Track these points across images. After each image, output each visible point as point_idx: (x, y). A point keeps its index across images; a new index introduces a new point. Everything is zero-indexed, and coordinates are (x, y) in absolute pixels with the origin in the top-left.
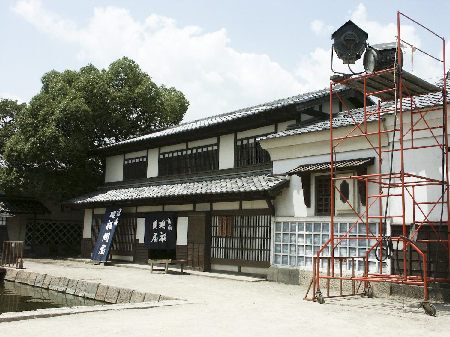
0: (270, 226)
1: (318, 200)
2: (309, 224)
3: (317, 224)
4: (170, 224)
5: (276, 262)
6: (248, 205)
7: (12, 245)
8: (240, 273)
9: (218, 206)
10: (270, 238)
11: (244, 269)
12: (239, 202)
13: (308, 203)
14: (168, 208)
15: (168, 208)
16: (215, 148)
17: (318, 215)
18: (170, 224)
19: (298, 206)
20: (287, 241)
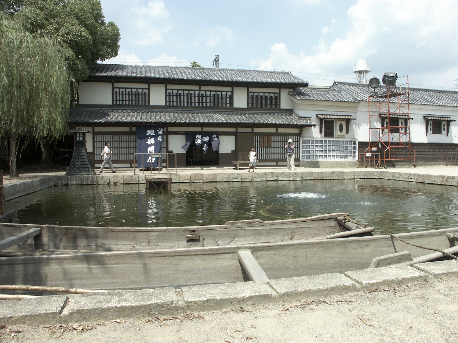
0: (299, 142)
1: (325, 130)
2: (321, 141)
3: (326, 141)
4: (161, 135)
5: (302, 158)
6: (281, 130)
7: (76, 138)
8: (277, 165)
9: (256, 130)
10: (299, 147)
11: (279, 164)
12: (204, 131)
13: (321, 132)
14: (206, 129)
15: (206, 129)
16: (229, 94)
17: (326, 137)
18: (161, 135)
19: (316, 133)
20: (392, 157)
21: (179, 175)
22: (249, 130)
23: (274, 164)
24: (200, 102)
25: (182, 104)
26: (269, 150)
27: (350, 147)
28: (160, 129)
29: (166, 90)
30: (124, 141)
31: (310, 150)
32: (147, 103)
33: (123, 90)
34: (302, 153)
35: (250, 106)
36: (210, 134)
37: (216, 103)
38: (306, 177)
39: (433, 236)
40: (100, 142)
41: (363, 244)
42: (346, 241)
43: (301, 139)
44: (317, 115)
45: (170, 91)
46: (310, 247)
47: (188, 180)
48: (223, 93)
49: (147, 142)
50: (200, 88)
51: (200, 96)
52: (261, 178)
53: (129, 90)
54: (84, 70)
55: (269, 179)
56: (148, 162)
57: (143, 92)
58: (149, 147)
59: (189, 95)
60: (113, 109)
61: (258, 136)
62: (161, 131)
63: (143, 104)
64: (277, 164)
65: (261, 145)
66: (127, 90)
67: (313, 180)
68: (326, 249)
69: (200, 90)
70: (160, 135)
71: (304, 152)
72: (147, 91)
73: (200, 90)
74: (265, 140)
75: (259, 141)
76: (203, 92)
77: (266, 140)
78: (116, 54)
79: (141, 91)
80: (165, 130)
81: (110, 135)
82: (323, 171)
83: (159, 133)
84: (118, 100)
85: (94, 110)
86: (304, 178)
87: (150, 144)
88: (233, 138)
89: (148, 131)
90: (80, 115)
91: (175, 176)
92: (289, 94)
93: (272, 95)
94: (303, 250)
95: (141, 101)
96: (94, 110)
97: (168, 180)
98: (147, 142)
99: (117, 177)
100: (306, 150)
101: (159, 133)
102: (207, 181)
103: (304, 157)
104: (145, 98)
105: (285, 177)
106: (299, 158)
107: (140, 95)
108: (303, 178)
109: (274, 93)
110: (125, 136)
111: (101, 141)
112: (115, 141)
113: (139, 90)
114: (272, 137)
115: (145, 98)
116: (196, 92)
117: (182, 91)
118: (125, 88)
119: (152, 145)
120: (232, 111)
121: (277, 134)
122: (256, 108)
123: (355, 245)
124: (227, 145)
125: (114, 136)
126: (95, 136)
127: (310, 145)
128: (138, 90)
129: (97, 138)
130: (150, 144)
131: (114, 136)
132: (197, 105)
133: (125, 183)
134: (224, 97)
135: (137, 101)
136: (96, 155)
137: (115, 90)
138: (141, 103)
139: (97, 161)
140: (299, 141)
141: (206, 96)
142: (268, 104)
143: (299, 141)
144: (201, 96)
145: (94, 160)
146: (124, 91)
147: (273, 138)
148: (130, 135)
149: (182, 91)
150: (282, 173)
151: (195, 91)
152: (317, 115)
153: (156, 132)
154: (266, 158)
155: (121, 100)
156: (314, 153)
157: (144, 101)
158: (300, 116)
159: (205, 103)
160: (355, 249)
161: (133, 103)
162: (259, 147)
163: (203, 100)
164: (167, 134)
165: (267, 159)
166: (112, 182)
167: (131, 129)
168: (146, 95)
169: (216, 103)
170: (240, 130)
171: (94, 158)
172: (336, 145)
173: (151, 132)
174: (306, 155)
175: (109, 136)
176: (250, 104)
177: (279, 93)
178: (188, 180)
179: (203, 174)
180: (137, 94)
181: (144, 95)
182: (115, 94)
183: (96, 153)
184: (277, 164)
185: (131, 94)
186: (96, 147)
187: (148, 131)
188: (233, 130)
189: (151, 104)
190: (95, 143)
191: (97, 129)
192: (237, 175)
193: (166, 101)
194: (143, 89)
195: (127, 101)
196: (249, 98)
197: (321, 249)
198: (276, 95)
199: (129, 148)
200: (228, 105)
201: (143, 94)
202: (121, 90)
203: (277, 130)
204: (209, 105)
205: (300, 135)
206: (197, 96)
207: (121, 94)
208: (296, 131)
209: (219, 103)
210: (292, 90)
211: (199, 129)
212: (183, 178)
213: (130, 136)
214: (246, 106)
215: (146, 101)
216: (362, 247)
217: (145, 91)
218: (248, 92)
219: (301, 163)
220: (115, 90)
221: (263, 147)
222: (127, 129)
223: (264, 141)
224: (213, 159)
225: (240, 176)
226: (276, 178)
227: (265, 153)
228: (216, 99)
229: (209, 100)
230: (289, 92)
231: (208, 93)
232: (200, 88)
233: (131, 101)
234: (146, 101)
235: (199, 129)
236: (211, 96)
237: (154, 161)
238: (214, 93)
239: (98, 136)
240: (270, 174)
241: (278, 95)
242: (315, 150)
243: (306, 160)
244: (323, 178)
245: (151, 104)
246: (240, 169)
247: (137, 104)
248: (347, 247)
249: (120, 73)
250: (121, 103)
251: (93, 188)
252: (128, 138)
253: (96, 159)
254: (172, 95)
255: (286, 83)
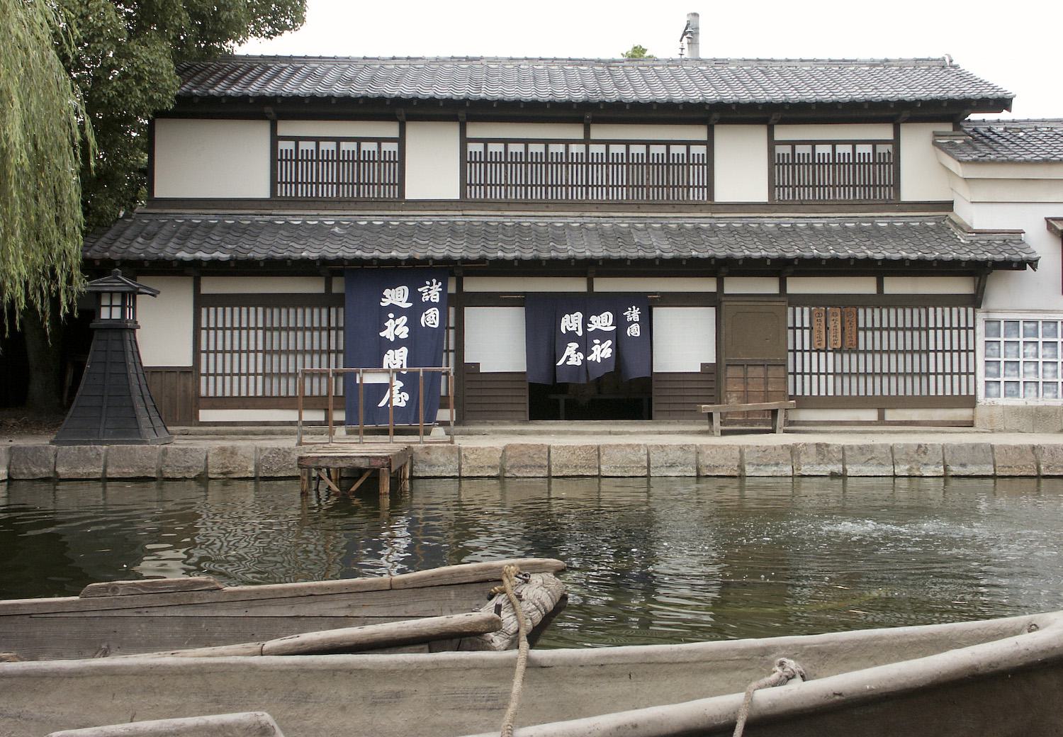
5: (987, 395)
6: (894, 286)
8: (881, 421)
9: (797, 286)
11: (890, 415)
14: (604, 285)
21: (459, 450)
22: (769, 286)
23: (872, 415)
24: (297, 183)
25: (520, 194)
26: (851, 362)
27: (1030, 346)
28: (431, 285)
29: (464, 141)
30: (304, 329)
31: (1021, 360)
32: (392, 192)
33: (311, 146)
34: (987, 374)
35: (780, 194)
36: (617, 303)
37: (648, 187)
38: (963, 465)
39: (705, 671)
40: (236, 333)
41: (381, 689)
42: (303, 670)
43: (981, 316)
44: (1047, 219)
45: (479, 147)
46: (149, 690)
47: (493, 467)
48: (675, 150)
49: (382, 334)
50: (587, 132)
51: (587, 161)
52: (777, 464)
53: (331, 146)
54: (156, 74)
55: (805, 470)
56: (382, 404)
57: (379, 152)
58: (390, 352)
59: (547, 161)
60: (275, 212)
61: (806, 310)
62: (433, 292)
63: (379, 193)
64: (881, 416)
65: (815, 341)
66: (324, 146)
67: (994, 477)
68: (217, 702)
69: (587, 141)
70: (430, 304)
71: (993, 369)
72: (394, 147)
73: (587, 141)
74: (831, 324)
75: (811, 329)
76: (601, 149)
77: (835, 323)
78: (299, 19)
79: (372, 147)
80: (452, 289)
81: (256, 306)
82: (1041, 443)
83: (425, 298)
84: (291, 183)
85: (204, 217)
86: (955, 470)
87: (392, 339)
88: (705, 316)
89: (387, 292)
90: (150, 237)
91: (443, 454)
92: (935, 144)
93: (867, 149)
94: (118, 702)
95: (374, 184)
96: (204, 217)
97: (379, 463)
98: (382, 334)
99: (233, 452)
100: (1002, 360)
101: (425, 298)
102: (565, 472)
103: (993, 390)
104: (389, 174)
105: (875, 461)
106: (972, 393)
107: (369, 161)
108: (952, 468)
109: (874, 143)
110: (308, 311)
111: (224, 329)
112: (272, 329)
113: (366, 146)
114: (861, 311)
115: (389, 174)
116: (574, 149)
117: (313, 144)
118: (317, 140)
119: (398, 343)
120: (709, 215)
121: (880, 301)
122: (802, 203)
123: (344, 693)
124: (684, 341)
125: (268, 311)
126: (204, 311)
127: (1021, 340)
128: (322, 144)
129: (211, 316)
130: (392, 339)
131: (268, 311)
132: (578, 194)
133: (261, 474)
134: (658, 164)
135: (359, 184)
136: (203, 379)
137: (283, 145)
138: (374, 193)
139: (207, 397)
140: (971, 325)
141: (609, 161)
142: (849, 186)
143: (971, 325)
144: (593, 164)
145: (198, 396)
146: (584, 152)
147: (866, 317)
148: (285, 306)
149: (375, 144)
150: (862, 449)
151: (567, 142)
152: (1047, 219)
153: (414, 297)
154: (839, 393)
155: (302, 183)
156: (1037, 373)
157: (385, 184)
158: (976, 227)
159: (607, 186)
160: (343, 708)
161: (345, 192)
162: (810, 351)
163: (598, 175)
164: (457, 302)
165: (936, 395)
166: (214, 472)
167: (328, 286)
168: (390, 162)
169: (648, 187)
170: (734, 286)
171: (199, 387)
172: (1040, 340)
173: (397, 296)
174: (1002, 379)
175: (236, 309)
176: (779, 186)
177: (896, 143)
178: (493, 467)
179: (549, 448)
180: (359, 160)
181: (385, 161)
182: (281, 160)
183: (203, 370)
184: (881, 416)
185: (338, 161)
186: (204, 348)
187: (387, 292)
188: (708, 286)
189: (409, 195)
190: (204, 333)
191: (211, 286)
192: (679, 453)
193: (464, 184)
194: (379, 141)
195: (572, 186)
196: (774, 162)
197: (193, 699)
198: (882, 149)
199: (320, 352)
200: (695, 195)
201: (382, 161)
202: (304, 146)
203: (880, 286)
204: (621, 194)
205: (975, 301)
206: (286, 160)
207: (491, 162)
208: (961, 286)
209: (658, 187)
210: (947, 128)
211: (577, 285)
212: (475, 460)
213: (300, 311)
214: (763, 197)
215: (389, 184)
216: (375, 704)
217: (386, 147)
218: (772, 144)
219: (981, 412)
220: (283, 145)
221: (826, 351)
222: (314, 286)
223: (827, 328)
224: (627, 394)
225: (692, 457)
226: (837, 468)
227: (835, 374)
228: (648, 173)
229: (621, 175)
230: (936, 135)
231: (618, 149)
232: (587, 132)
233: (338, 184)
234: (389, 184)
235: (577, 285)
236: (628, 162)
237: (403, 404)
238: (640, 149)
239: (252, 309)
240: (814, 450)
241: (890, 147)
242: (1041, 360)
243: (1003, 401)
244: (1038, 469)
245: (409, 195)
246: (724, 433)
247: (358, 193)
248: (305, 698)
249: (304, 88)
250: (303, 191)
251: (160, 488)
252: (317, 316)
253: (203, 393)
254: (486, 162)
255: (917, 101)
